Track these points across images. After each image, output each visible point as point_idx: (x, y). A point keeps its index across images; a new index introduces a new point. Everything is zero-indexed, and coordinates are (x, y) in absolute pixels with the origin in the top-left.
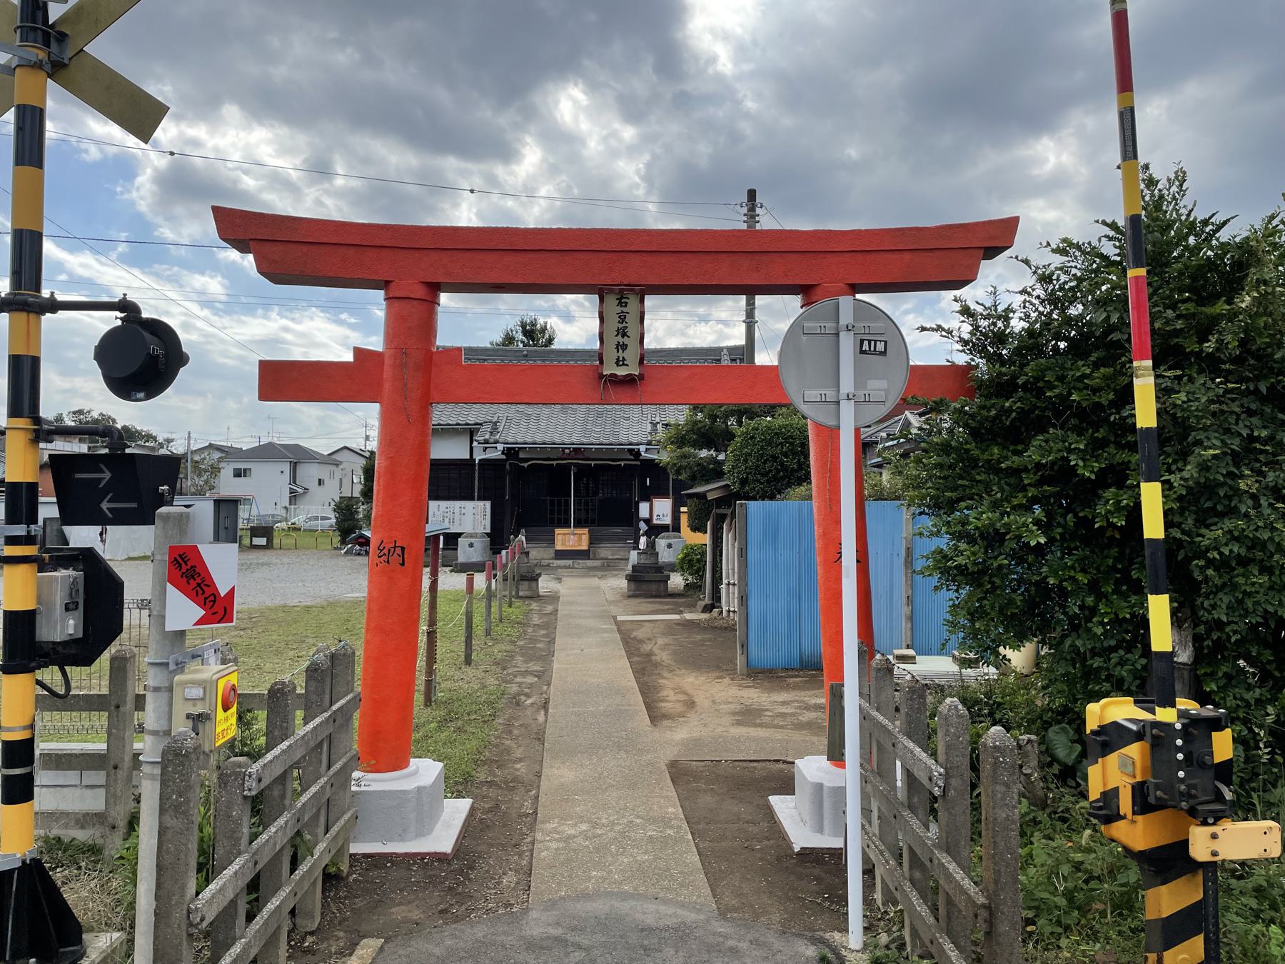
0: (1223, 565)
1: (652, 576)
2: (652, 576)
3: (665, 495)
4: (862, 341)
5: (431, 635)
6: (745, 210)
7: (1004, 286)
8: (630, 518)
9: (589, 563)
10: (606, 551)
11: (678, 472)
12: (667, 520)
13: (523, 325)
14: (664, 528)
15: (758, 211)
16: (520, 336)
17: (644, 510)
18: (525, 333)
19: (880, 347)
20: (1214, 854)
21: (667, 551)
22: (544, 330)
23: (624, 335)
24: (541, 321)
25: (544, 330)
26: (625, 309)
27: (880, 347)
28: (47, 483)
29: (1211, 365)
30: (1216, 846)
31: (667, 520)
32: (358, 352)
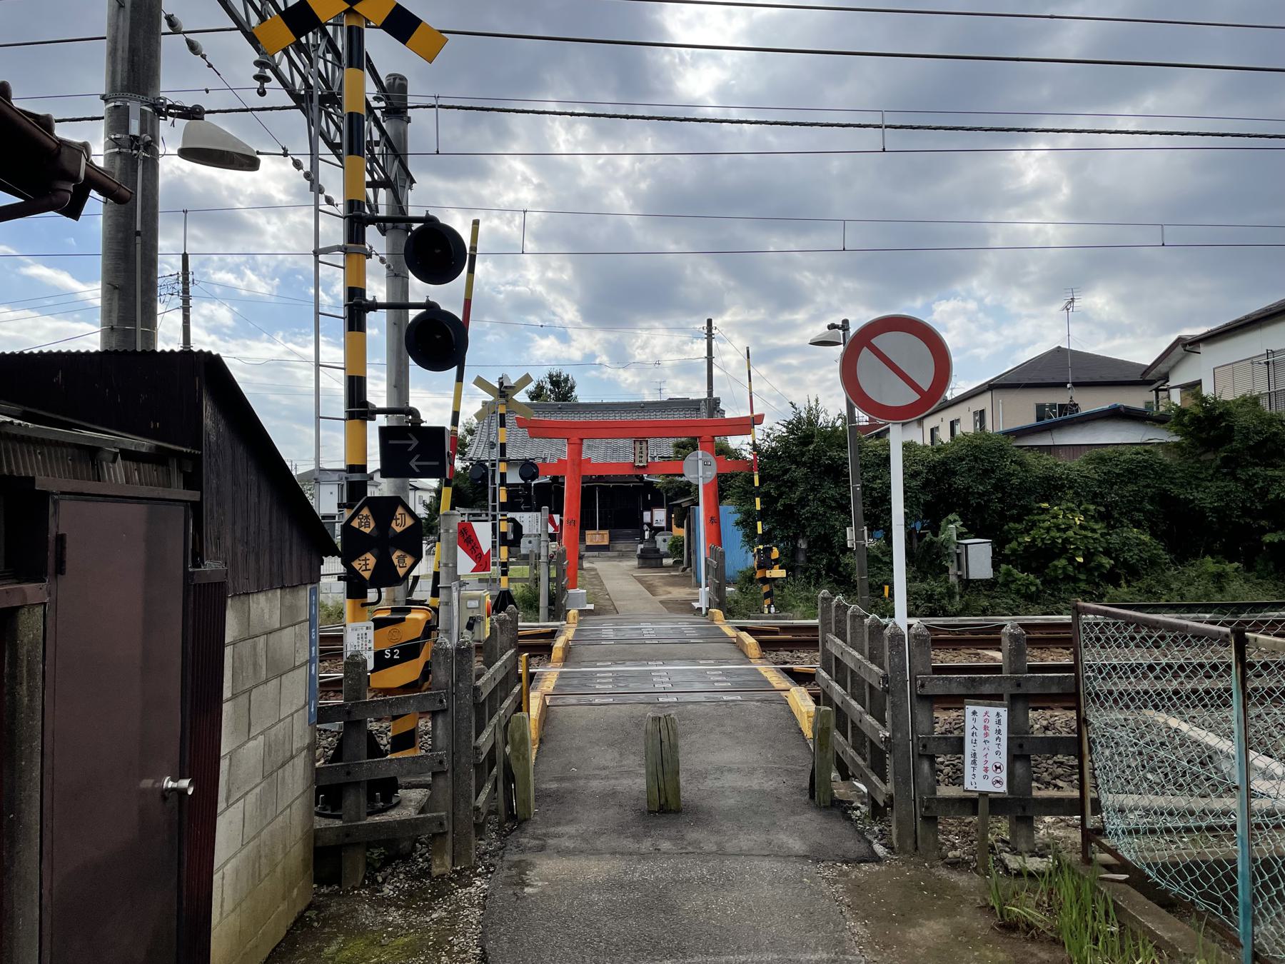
0: (807, 519)
1: (653, 555)
2: (653, 555)
3: (661, 506)
5: (180, 864)
7: (759, 433)
8: (637, 523)
9: (610, 554)
10: (621, 546)
11: (667, 492)
12: (664, 524)
13: (551, 376)
14: (661, 529)
16: (549, 386)
17: (647, 516)
18: (552, 383)
21: (662, 543)
22: (567, 380)
24: (564, 375)
25: (567, 380)
29: (804, 464)
31: (664, 524)
32: (559, 460)
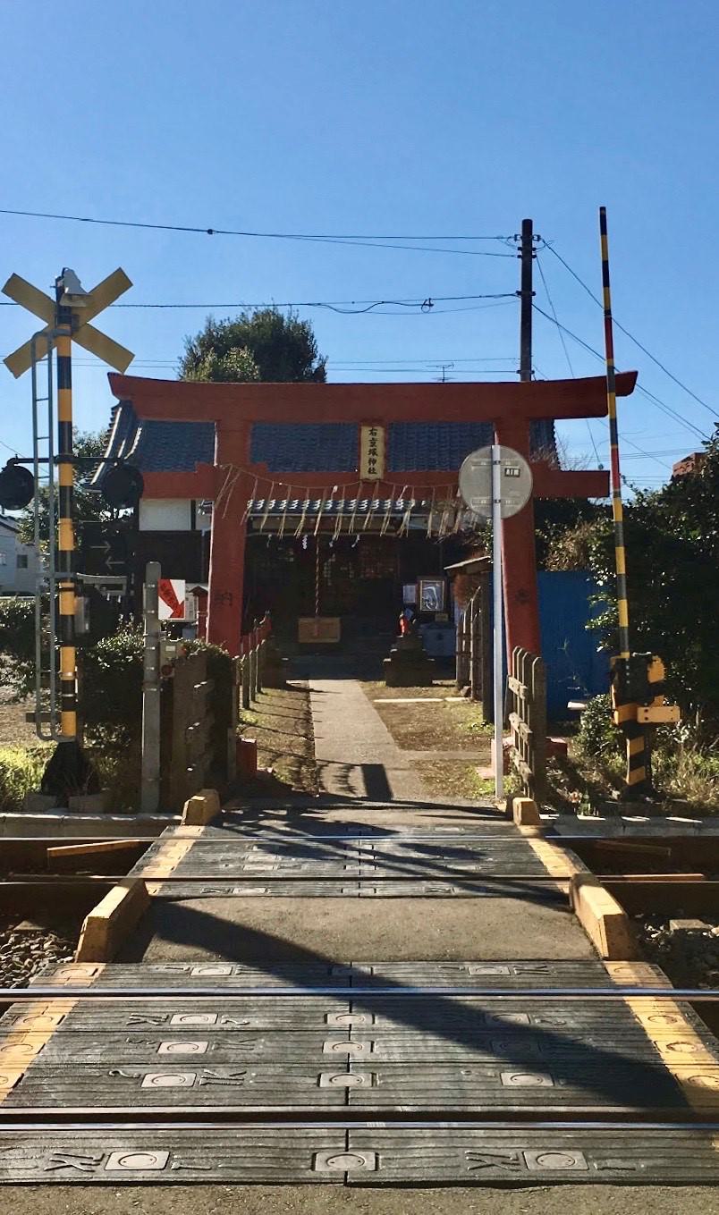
4: (506, 470)
6: (520, 243)
15: (535, 244)
17: (409, 591)
19: (516, 472)
20: (646, 719)
23: (374, 454)
26: (375, 437)
27: (516, 472)
28: (438, 524)
30: (647, 715)
